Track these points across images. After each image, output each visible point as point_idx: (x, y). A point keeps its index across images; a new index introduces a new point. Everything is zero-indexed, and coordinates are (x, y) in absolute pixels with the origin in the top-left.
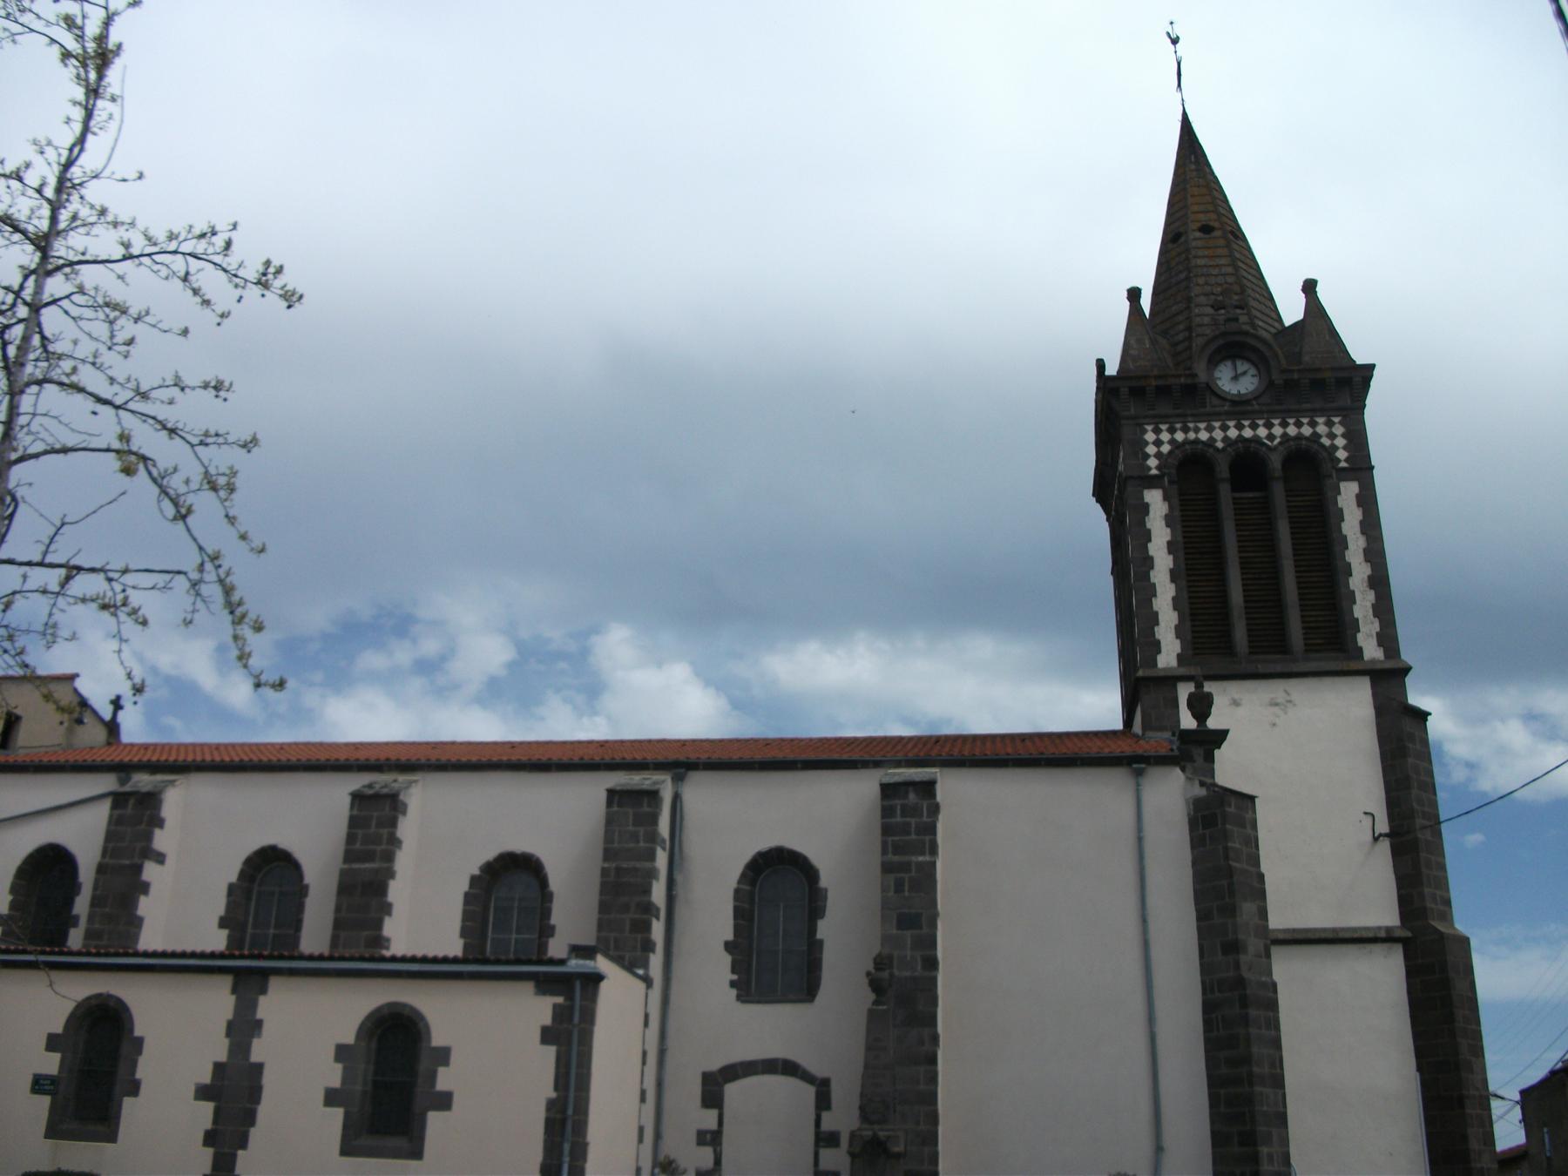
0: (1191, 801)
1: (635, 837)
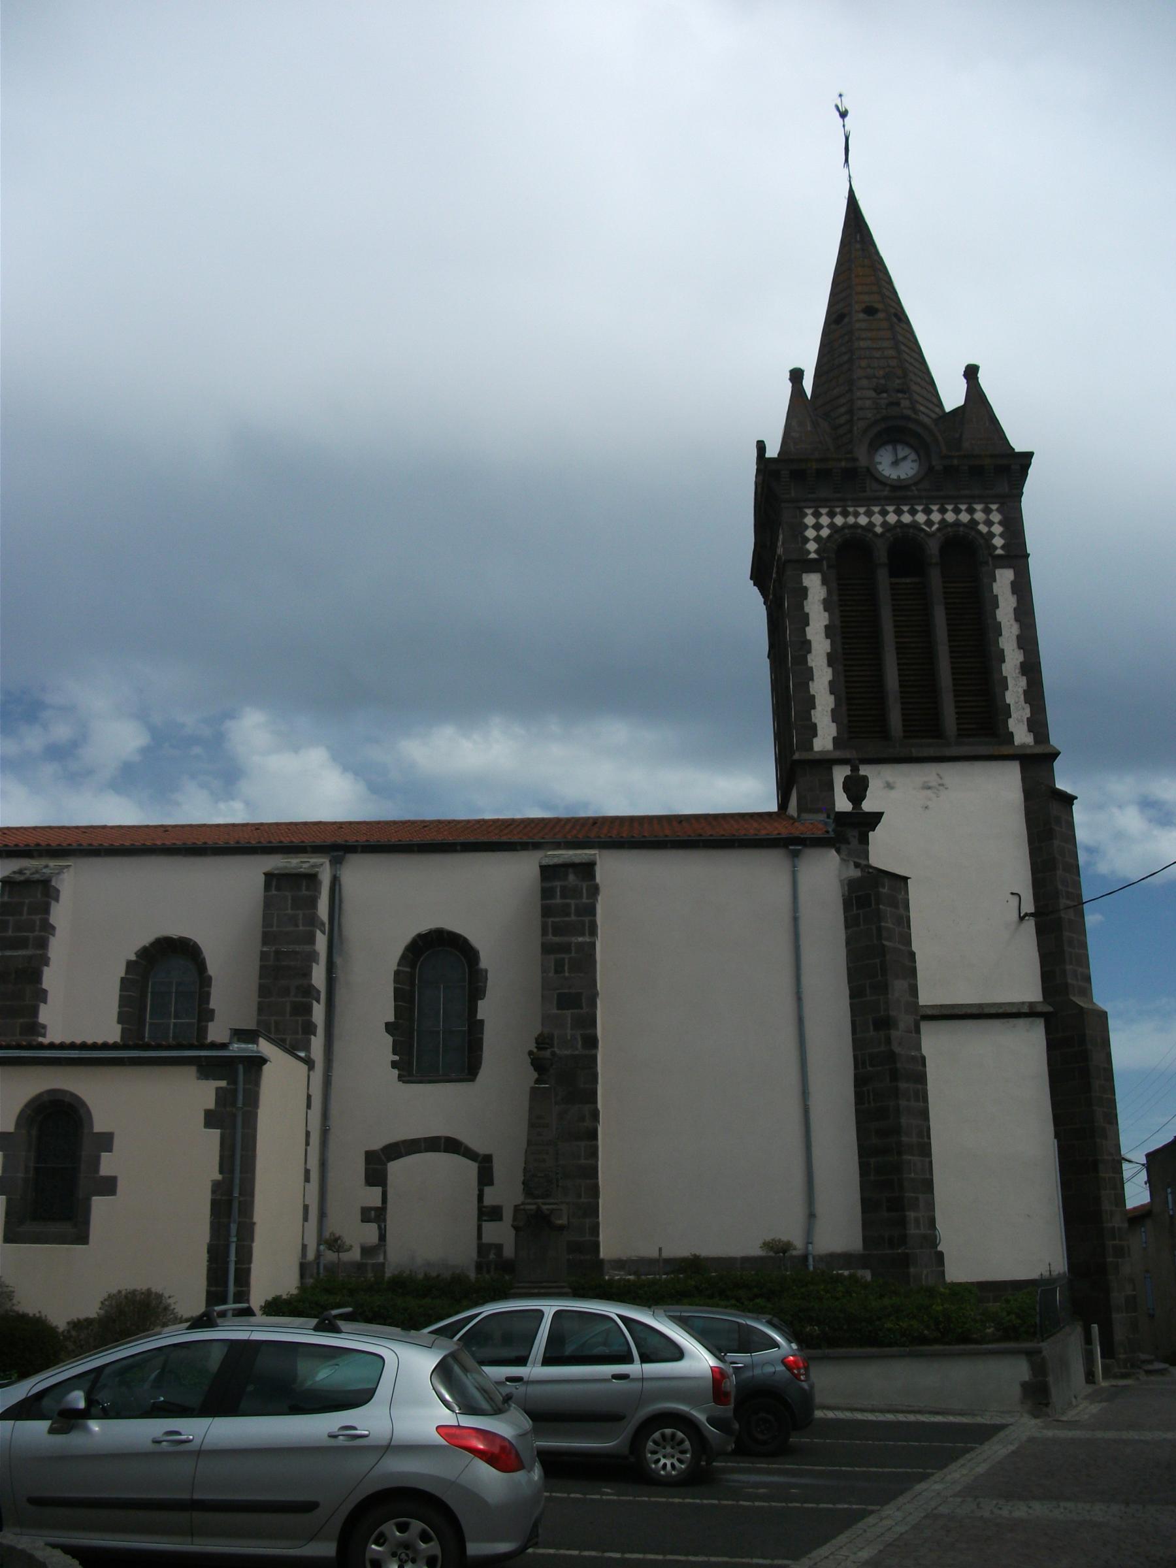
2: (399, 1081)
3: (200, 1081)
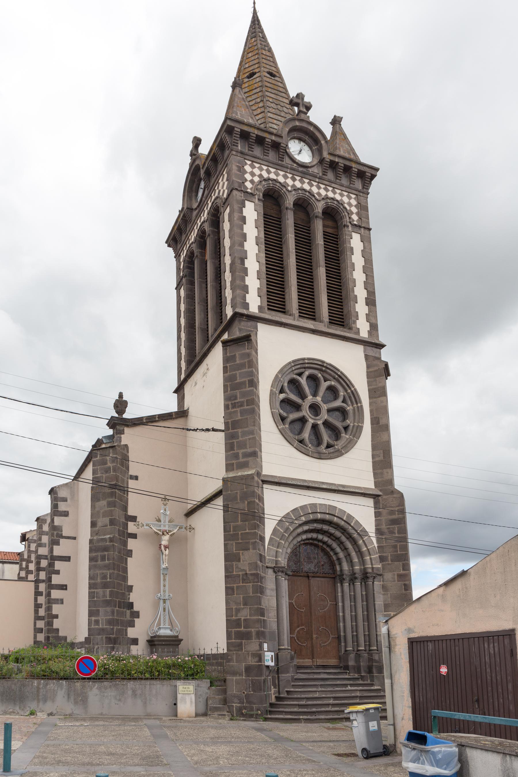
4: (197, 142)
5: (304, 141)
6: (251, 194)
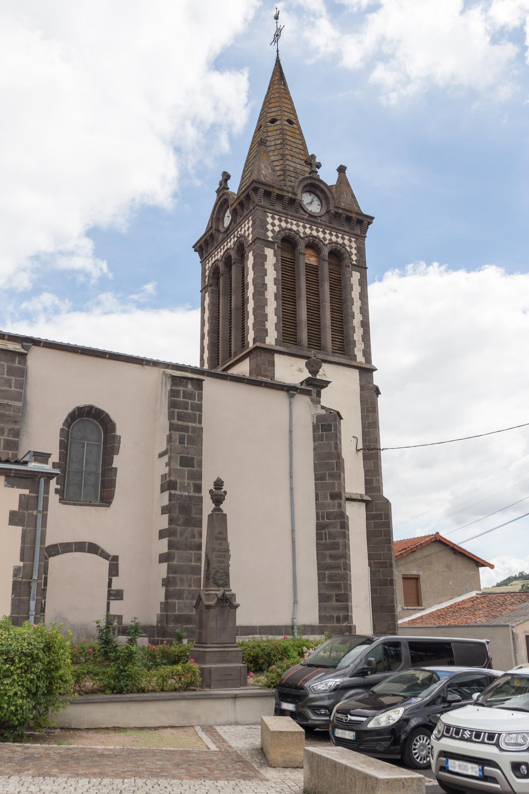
0: (315, 416)
1: (8, 383)
2: (60, 502)
3: (7, 488)
4: (226, 177)
5: (314, 193)
6: (271, 242)
